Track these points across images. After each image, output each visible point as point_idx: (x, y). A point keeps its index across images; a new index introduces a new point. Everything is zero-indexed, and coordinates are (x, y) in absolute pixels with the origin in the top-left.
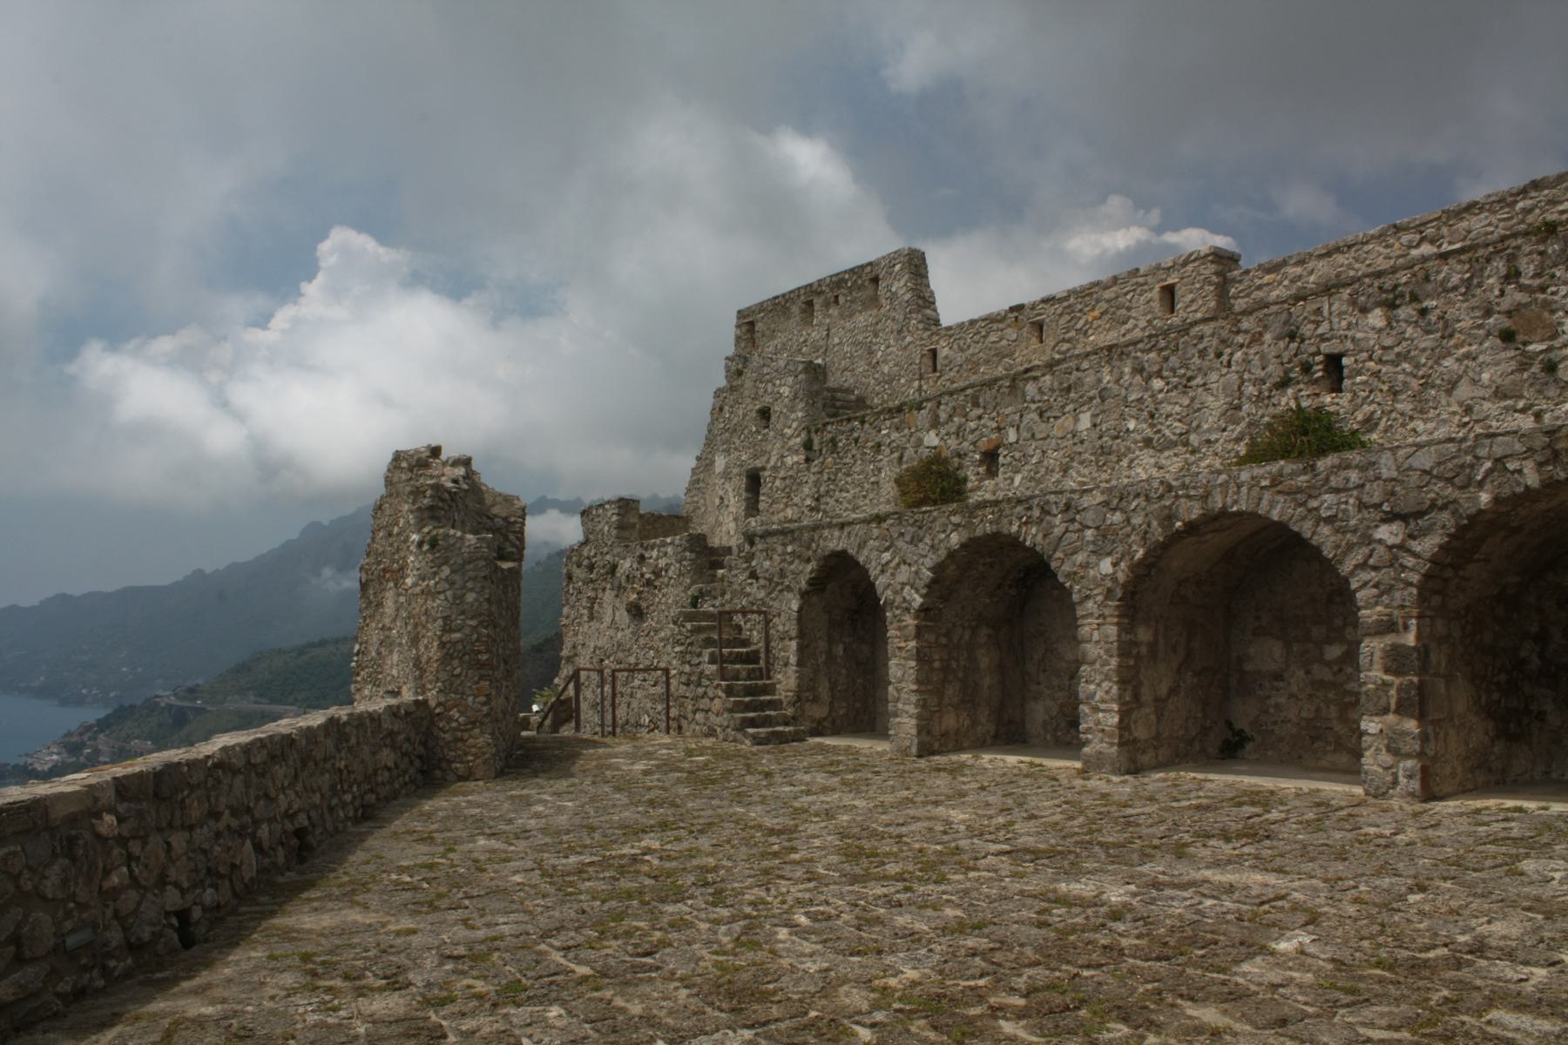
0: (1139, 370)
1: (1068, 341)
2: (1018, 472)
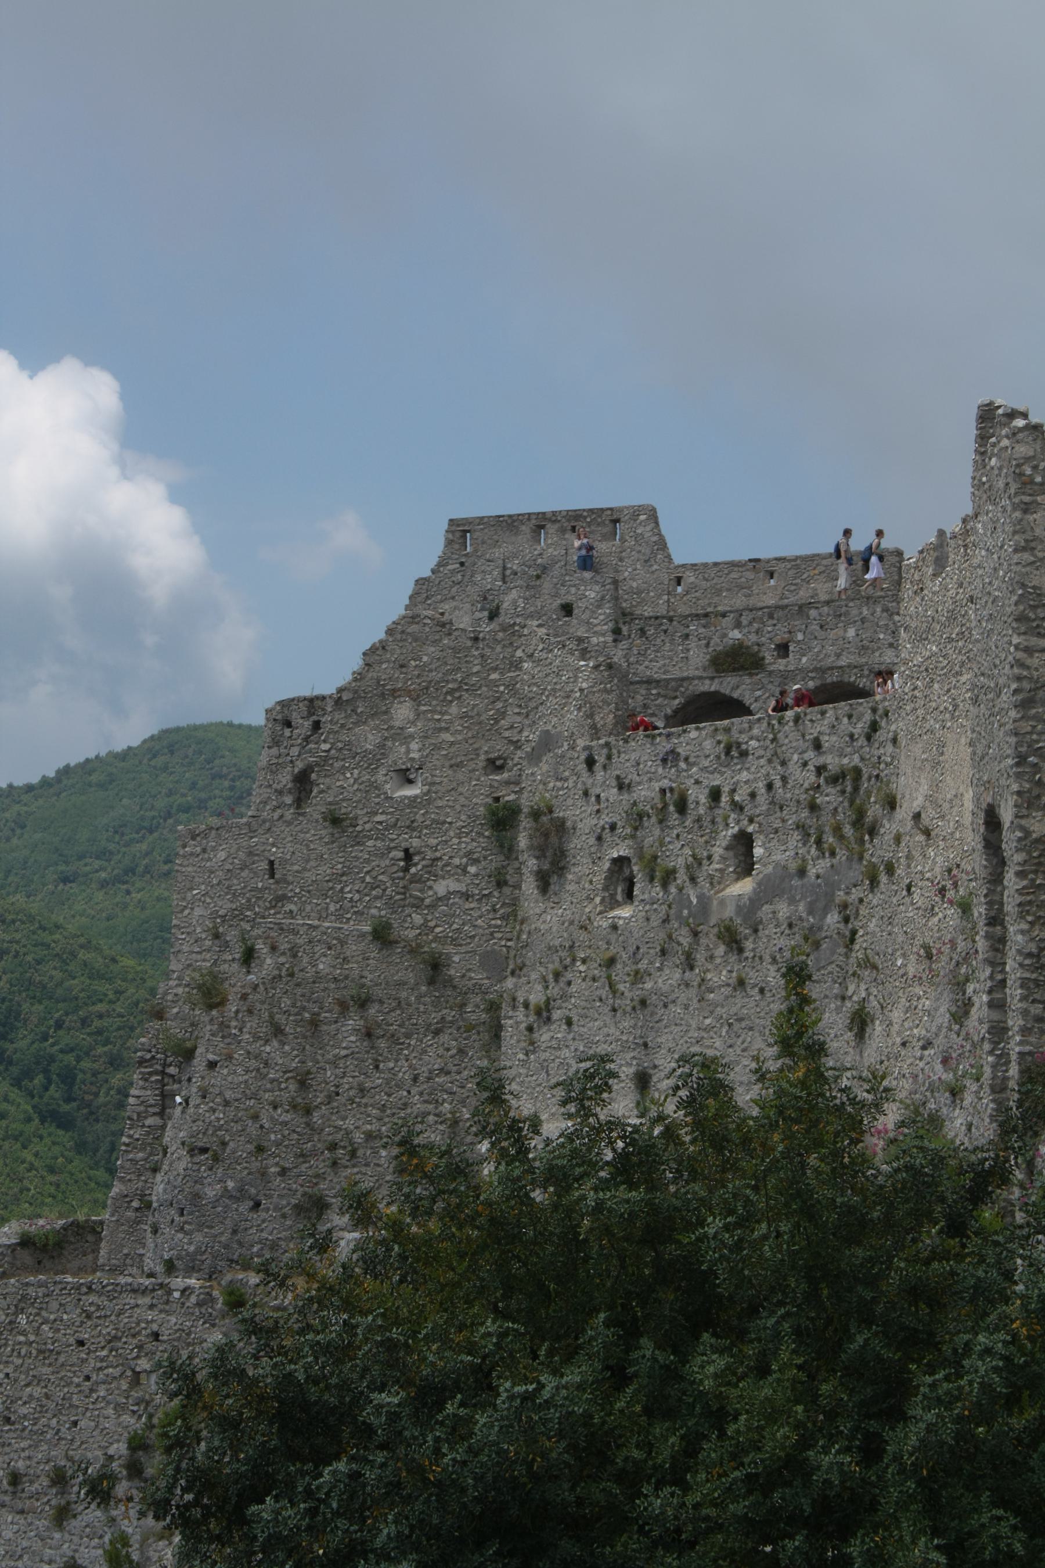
0: (886, 610)
1: (795, 585)
2: (804, 655)
